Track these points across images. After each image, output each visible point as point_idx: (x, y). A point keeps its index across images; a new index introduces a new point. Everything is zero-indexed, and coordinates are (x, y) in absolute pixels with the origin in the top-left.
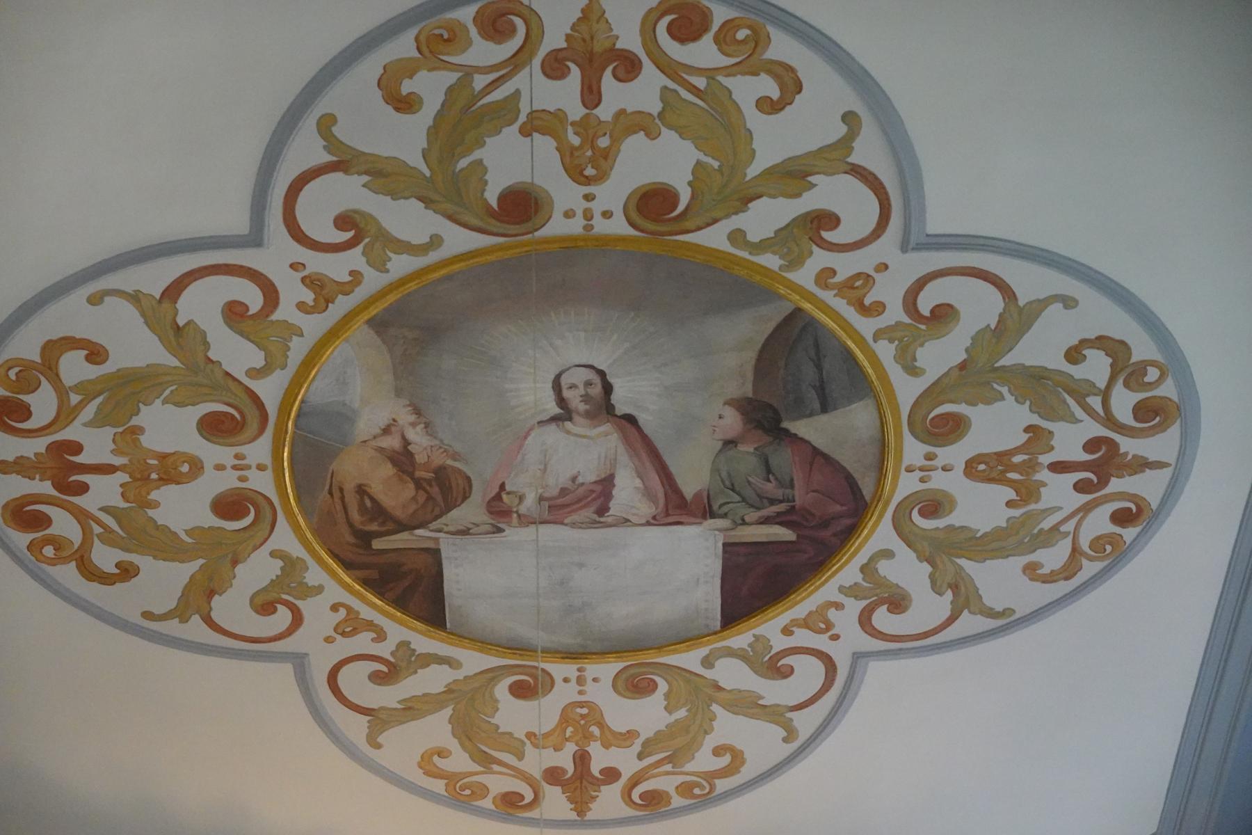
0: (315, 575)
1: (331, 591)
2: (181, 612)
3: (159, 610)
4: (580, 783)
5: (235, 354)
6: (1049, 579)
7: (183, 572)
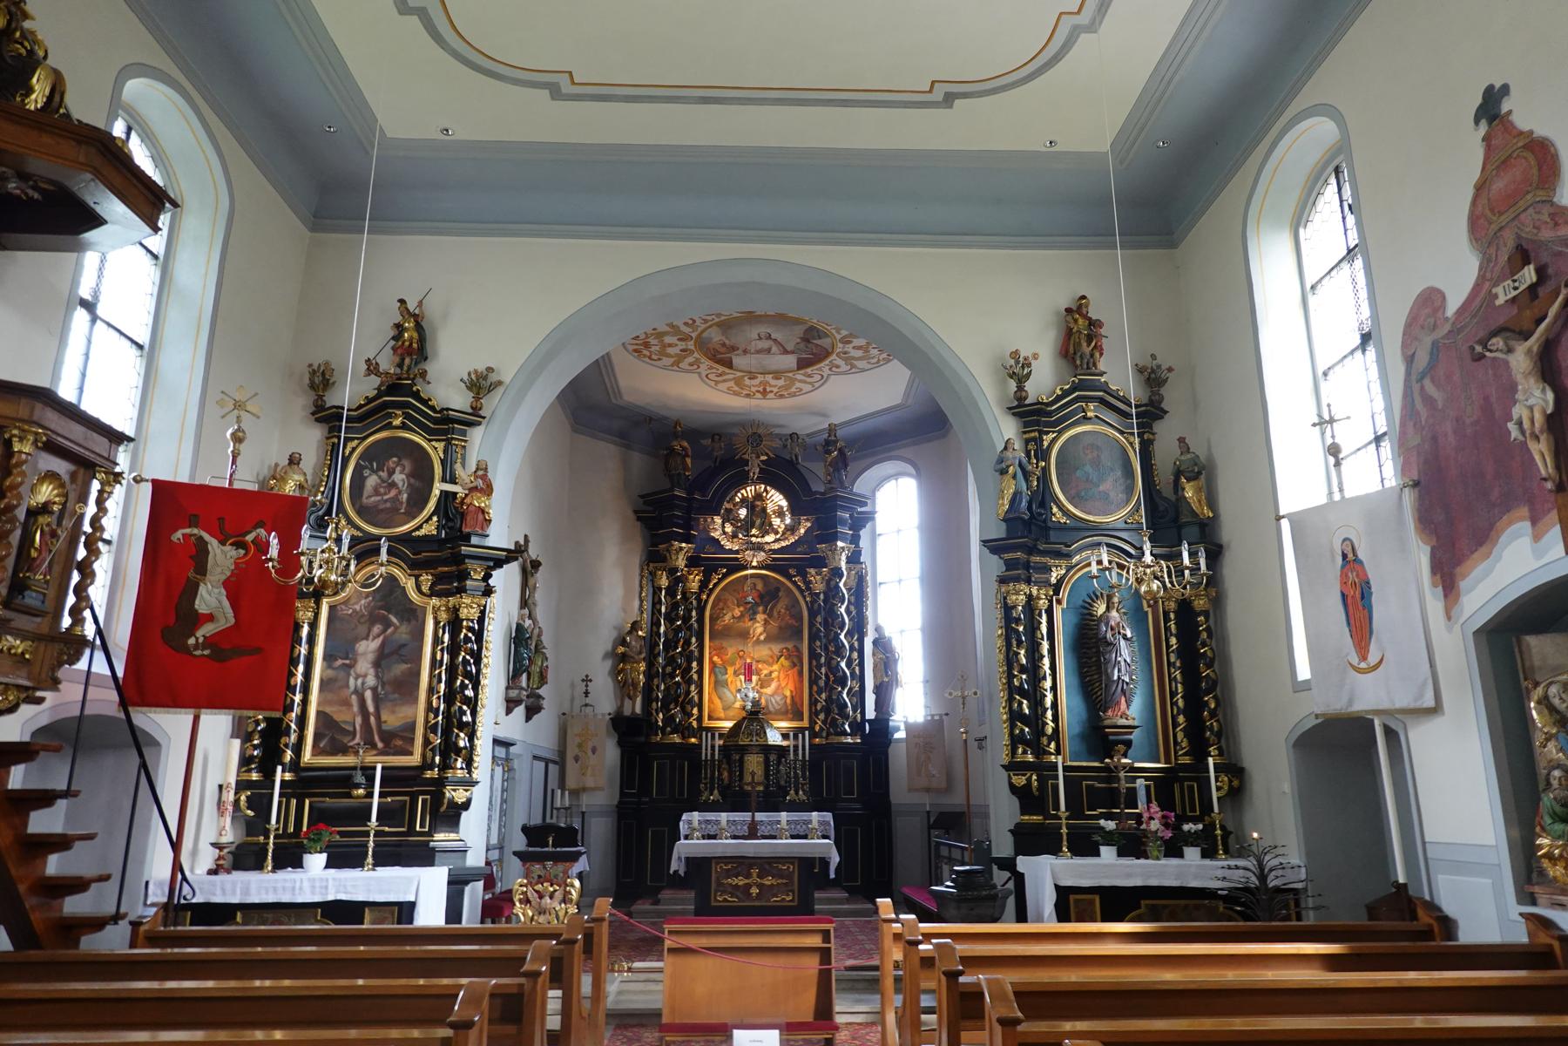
1: (706, 363)
4: (764, 393)
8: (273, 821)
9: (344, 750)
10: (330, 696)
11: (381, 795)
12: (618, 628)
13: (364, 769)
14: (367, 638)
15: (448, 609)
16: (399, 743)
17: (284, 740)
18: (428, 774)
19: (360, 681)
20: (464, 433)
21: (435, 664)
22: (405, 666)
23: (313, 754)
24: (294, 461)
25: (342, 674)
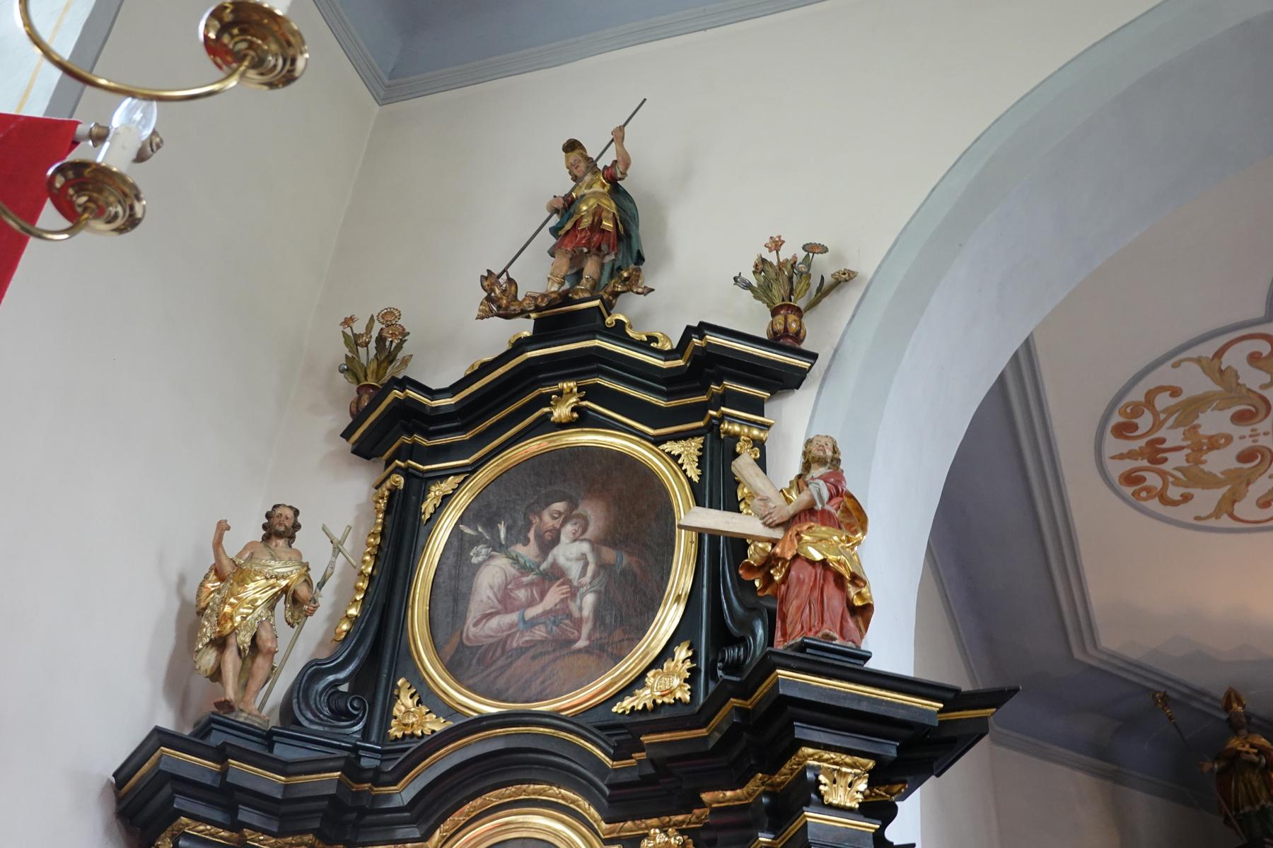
2: (1216, 514)
3: (1204, 515)
6: (1161, 389)
7: (1218, 494)
20: (756, 406)
24: (280, 529)
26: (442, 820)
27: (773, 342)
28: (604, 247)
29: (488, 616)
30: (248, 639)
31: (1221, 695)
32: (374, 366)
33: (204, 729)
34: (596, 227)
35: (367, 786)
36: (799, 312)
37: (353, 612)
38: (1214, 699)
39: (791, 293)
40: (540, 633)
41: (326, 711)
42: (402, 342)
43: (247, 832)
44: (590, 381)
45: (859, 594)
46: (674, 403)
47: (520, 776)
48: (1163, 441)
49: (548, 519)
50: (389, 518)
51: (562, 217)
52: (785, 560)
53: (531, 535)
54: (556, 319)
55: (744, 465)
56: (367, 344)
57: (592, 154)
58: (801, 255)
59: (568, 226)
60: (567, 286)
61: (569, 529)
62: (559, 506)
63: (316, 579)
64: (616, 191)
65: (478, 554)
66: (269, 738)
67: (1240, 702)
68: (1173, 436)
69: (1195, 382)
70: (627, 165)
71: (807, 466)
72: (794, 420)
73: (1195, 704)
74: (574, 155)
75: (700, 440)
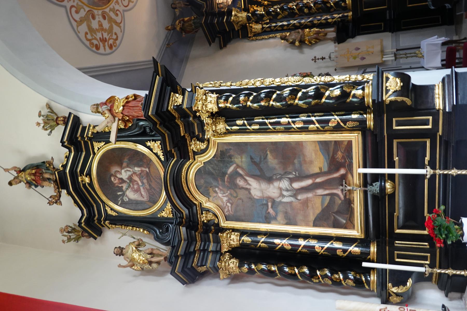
0: (111, 7)
2: (120, 27)
3: (120, 30)
5: (83, 13)
6: (86, 37)
7: (115, 27)
8: (422, 269)
9: (349, 202)
10: (300, 217)
11: (392, 166)
12: (286, 48)
13: (365, 184)
14: (248, 190)
15: (215, 123)
16: (339, 155)
17: (339, 253)
18: (370, 123)
19: (285, 193)
20: (84, 128)
21: (263, 130)
22: (269, 156)
23: (353, 228)
24: (120, 252)
25: (280, 208)
26: (191, 201)
27: (66, 124)
28: (40, 172)
29: (142, 195)
30: (149, 255)
31: (167, 31)
32: (76, 233)
33: (171, 263)
34: (34, 174)
35: (184, 220)
36: (57, 118)
37: (142, 230)
38: (168, 33)
39: (53, 120)
40: (145, 181)
41: (166, 234)
42: (69, 226)
43: (196, 249)
44: (79, 173)
45: (131, 97)
46: (84, 150)
47: (180, 182)
48: (100, 38)
49: (116, 181)
50: (117, 224)
51: (32, 185)
52: (123, 116)
53: (120, 185)
54: (61, 184)
55: (98, 129)
56: (70, 236)
57: (12, 178)
58: (42, 118)
59: (34, 182)
60: (52, 182)
61: (118, 176)
62: (112, 179)
63: (133, 240)
64: (24, 170)
65: (126, 199)
66: (173, 247)
67: (168, 27)
68: (99, 35)
69: (84, 28)
70: (16, 167)
71: (99, 112)
72: (88, 118)
73: (169, 38)
74: (13, 183)
75: (94, 142)
